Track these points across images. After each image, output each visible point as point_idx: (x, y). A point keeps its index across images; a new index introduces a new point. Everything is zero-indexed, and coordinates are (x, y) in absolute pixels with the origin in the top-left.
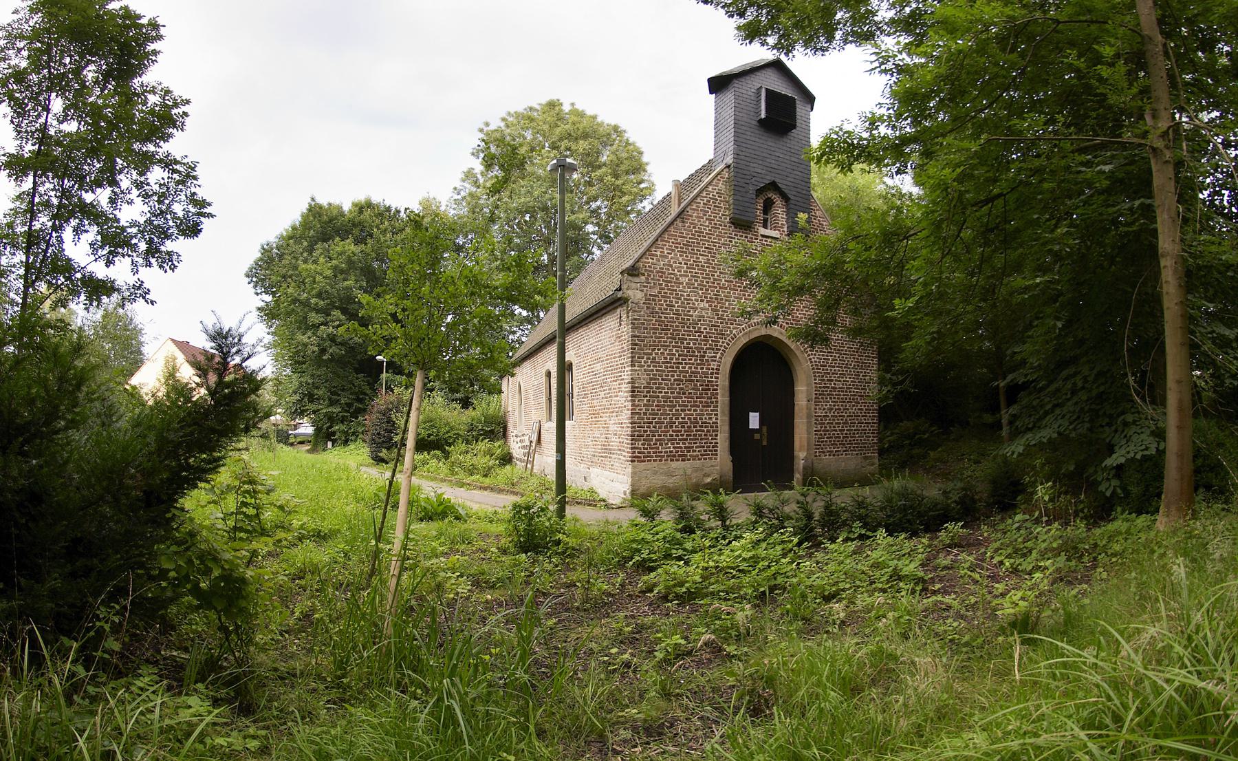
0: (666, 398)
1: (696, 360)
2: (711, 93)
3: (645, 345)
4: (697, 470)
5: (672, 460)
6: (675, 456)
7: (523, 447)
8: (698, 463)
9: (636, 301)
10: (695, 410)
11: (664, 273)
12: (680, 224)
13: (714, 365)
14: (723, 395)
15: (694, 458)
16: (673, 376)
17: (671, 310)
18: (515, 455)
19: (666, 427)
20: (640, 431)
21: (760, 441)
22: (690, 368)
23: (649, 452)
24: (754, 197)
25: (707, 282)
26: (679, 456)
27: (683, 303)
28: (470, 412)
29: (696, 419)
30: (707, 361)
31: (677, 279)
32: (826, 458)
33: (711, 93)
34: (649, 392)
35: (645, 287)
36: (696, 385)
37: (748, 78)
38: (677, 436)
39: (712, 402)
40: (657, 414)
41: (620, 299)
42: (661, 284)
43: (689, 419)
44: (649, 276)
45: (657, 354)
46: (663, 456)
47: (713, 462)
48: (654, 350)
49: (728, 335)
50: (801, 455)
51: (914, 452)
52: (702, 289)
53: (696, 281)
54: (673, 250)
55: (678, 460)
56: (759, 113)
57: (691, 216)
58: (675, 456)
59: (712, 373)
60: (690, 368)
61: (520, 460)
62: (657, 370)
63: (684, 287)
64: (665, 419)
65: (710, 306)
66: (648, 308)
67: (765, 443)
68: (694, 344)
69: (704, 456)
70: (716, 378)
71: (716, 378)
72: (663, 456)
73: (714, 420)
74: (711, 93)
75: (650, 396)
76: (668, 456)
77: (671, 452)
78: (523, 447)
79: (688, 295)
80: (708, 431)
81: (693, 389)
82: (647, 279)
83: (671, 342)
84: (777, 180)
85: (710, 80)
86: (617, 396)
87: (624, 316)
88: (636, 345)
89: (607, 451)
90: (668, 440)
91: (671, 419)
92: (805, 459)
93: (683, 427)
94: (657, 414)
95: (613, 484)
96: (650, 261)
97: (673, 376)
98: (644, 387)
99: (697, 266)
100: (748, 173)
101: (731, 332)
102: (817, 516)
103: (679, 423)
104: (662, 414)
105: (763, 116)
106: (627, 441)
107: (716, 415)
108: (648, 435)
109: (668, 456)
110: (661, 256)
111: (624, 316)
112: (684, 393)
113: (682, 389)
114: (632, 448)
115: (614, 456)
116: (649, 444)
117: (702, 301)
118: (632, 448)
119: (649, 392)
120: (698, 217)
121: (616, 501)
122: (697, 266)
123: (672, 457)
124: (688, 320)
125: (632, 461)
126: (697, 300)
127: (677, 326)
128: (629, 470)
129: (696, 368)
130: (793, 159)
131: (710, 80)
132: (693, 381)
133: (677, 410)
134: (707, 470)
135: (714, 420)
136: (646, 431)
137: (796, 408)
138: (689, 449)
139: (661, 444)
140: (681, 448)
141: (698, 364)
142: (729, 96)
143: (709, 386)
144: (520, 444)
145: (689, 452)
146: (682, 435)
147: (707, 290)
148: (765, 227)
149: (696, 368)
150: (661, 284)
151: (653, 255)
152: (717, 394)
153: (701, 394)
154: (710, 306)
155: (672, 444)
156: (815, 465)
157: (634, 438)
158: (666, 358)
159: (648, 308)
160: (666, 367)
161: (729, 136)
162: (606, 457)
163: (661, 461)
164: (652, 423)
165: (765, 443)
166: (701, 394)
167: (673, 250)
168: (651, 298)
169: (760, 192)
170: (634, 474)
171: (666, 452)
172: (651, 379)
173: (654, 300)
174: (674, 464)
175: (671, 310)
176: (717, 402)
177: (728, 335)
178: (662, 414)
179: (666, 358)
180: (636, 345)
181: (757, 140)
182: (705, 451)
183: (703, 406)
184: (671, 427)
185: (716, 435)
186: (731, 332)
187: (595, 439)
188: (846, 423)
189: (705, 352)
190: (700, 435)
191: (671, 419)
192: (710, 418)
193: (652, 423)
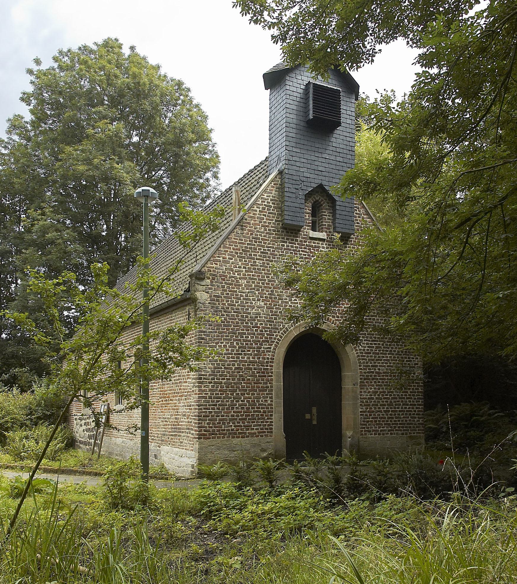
0: (228, 384)
1: (254, 351)
2: (266, 89)
3: (210, 340)
4: (254, 445)
5: (233, 437)
6: (235, 434)
7: (88, 430)
8: (256, 440)
9: (202, 302)
10: (253, 394)
11: (226, 276)
12: (239, 232)
13: (269, 355)
14: (277, 381)
15: (252, 435)
16: (234, 365)
17: (232, 309)
18: (78, 436)
19: (227, 409)
20: (206, 412)
21: (311, 420)
22: (249, 358)
23: (214, 431)
24: (303, 201)
25: (263, 284)
26: (240, 433)
27: (242, 302)
28: (27, 396)
29: (254, 401)
30: (263, 352)
31: (237, 281)
32: (371, 437)
33: (266, 89)
34: (213, 379)
35: (210, 289)
36: (253, 373)
37: (298, 72)
38: (238, 416)
39: (267, 387)
40: (220, 398)
41: (189, 299)
42: (223, 287)
43: (248, 401)
44: (214, 279)
45: (220, 346)
46: (225, 434)
47: (269, 439)
48: (217, 343)
49: (281, 329)
50: (348, 434)
51: (469, 434)
52: (258, 290)
53: (253, 282)
54: (234, 256)
55: (238, 437)
56: (306, 112)
57: (249, 223)
58: (235, 434)
59: (267, 362)
60: (249, 358)
61: (85, 443)
62: (220, 361)
63: (243, 289)
64: (228, 401)
65: (266, 304)
66: (212, 307)
67: (315, 422)
68: (252, 337)
69: (261, 433)
70: (271, 366)
71: (271, 366)
72: (225, 434)
73: (269, 402)
74: (266, 89)
75: (215, 383)
76: (230, 434)
77: (232, 430)
78: (88, 430)
79: (247, 296)
80: (264, 412)
81: (251, 376)
82: (212, 282)
83: (232, 337)
84: (324, 183)
85: (266, 76)
86: (186, 382)
87: (192, 314)
88: (203, 339)
89: (177, 430)
90: (230, 420)
91: (232, 401)
92: (352, 437)
93: (243, 408)
94: (220, 398)
95: (182, 459)
96: (214, 265)
97: (234, 365)
98: (210, 375)
99: (254, 269)
100: (298, 178)
101: (284, 326)
102: (345, 480)
103: (240, 405)
104: (224, 398)
105: (311, 117)
106: (194, 422)
107: (271, 398)
108: (213, 416)
109: (230, 434)
110: (224, 262)
111: (192, 314)
112: (243, 380)
113: (242, 376)
114: (199, 427)
115: (183, 434)
116: (214, 424)
117: (259, 300)
118: (199, 427)
119: (213, 379)
120: (255, 224)
121: (187, 475)
122: (254, 269)
123: (233, 434)
124: (247, 317)
125: (199, 438)
126: (254, 300)
127: (237, 323)
128: (197, 446)
129: (254, 358)
130: (338, 159)
131: (265, 76)
132: (251, 369)
133: (238, 394)
134: (264, 446)
135: (269, 402)
136: (211, 412)
137: (343, 391)
138: (248, 427)
139: (224, 424)
140: (241, 426)
141: (255, 355)
142: (281, 95)
143: (265, 373)
144: (84, 427)
145: (248, 429)
146: (242, 415)
147: (263, 290)
148: (314, 229)
149: (253, 358)
150: (223, 287)
151: (217, 261)
152: (272, 380)
153: (258, 380)
154: (266, 304)
155: (234, 423)
156: (361, 443)
157: (201, 418)
158: (227, 350)
159: (212, 307)
160: (228, 358)
161: (281, 140)
162: (175, 435)
163: (223, 437)
164: (216, 405)
165: (315, 422)
166: (258, 380)
167: (234, 256)
168: (214, 299)
169: (308, 196)
170: (200, 450)
171: (228, 430)
172: (215, 368)
173: (218, 301)
174: (236, 441)
175: (232, 309)
176: (272, 387)
177: (281, 329)
178: (224, 398)
179: (227, 350)
180: (203, 339)
181: (306, 143)
182: (262, 429)
183: (260, 391)
184: (233, 408)
185: (271, 415)
186: (284, 326)
187: (165, 420)
188: (391, 404)
189: (261, 345)
190: (258, 415)
191: (232, 401)
192: (266, 401)
193: (216, 405)
